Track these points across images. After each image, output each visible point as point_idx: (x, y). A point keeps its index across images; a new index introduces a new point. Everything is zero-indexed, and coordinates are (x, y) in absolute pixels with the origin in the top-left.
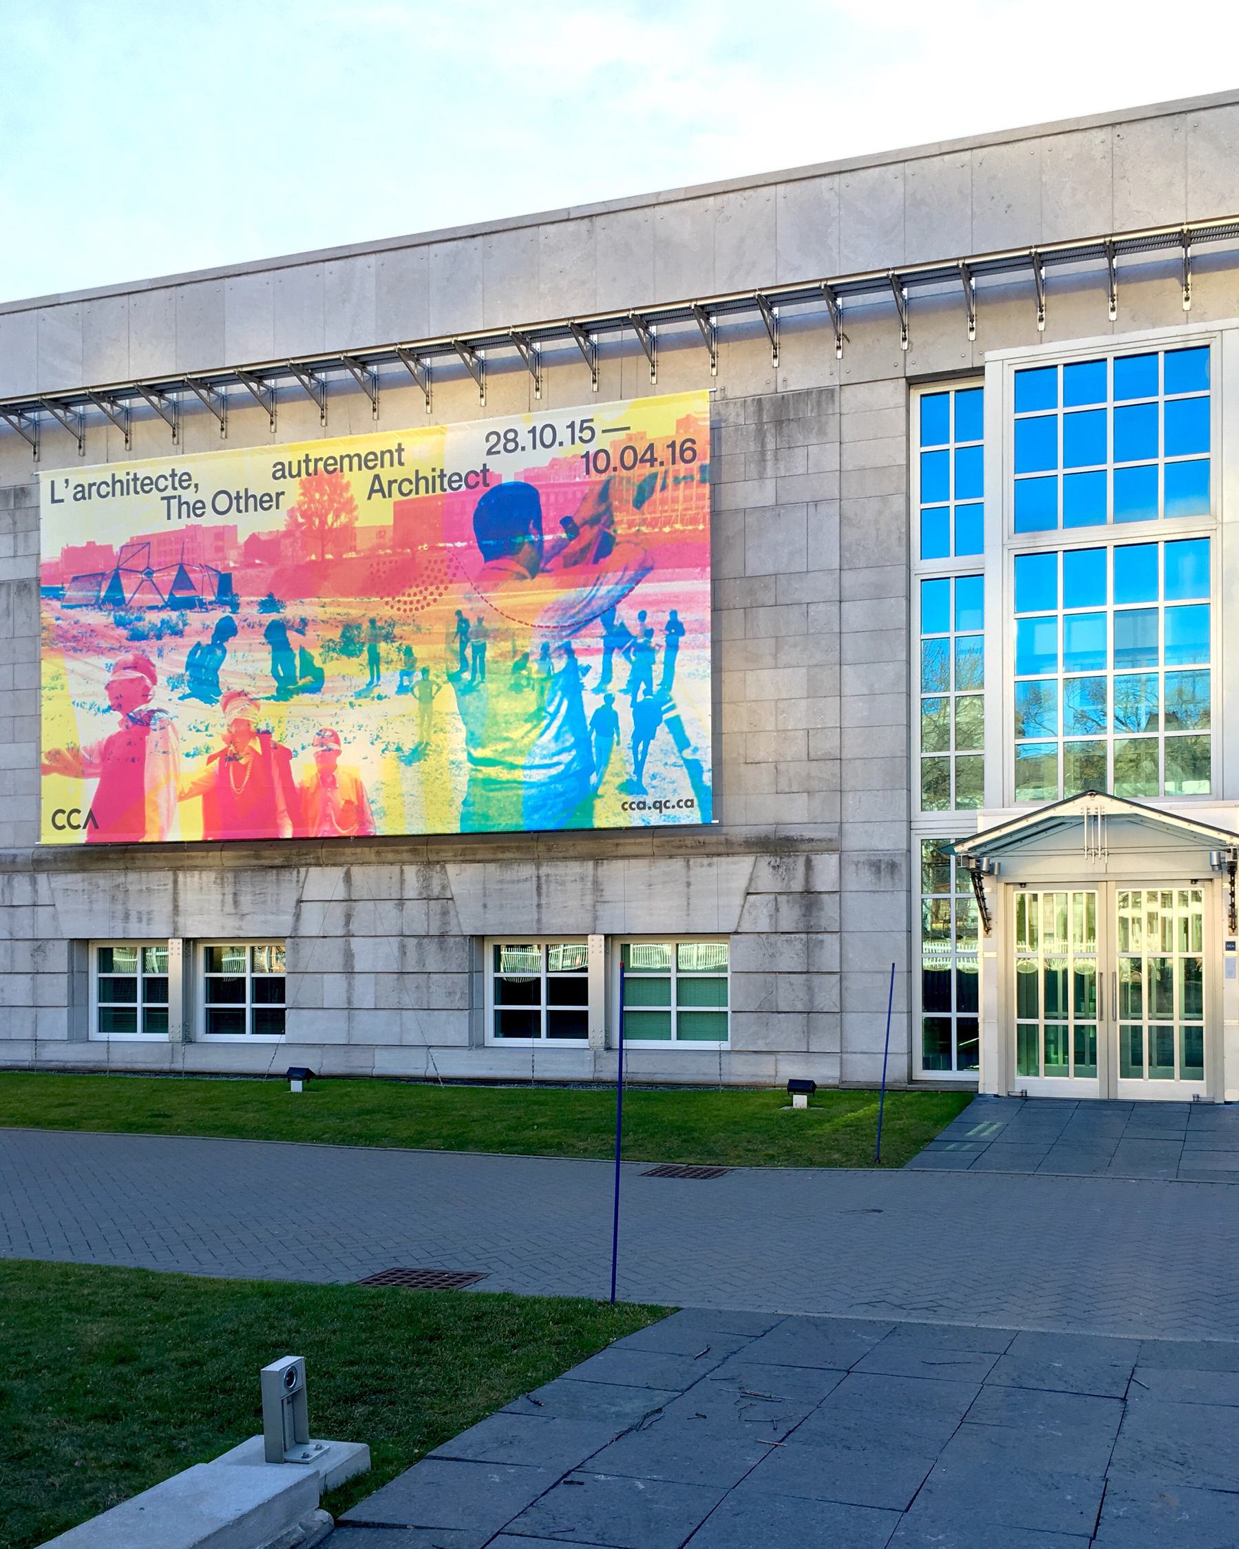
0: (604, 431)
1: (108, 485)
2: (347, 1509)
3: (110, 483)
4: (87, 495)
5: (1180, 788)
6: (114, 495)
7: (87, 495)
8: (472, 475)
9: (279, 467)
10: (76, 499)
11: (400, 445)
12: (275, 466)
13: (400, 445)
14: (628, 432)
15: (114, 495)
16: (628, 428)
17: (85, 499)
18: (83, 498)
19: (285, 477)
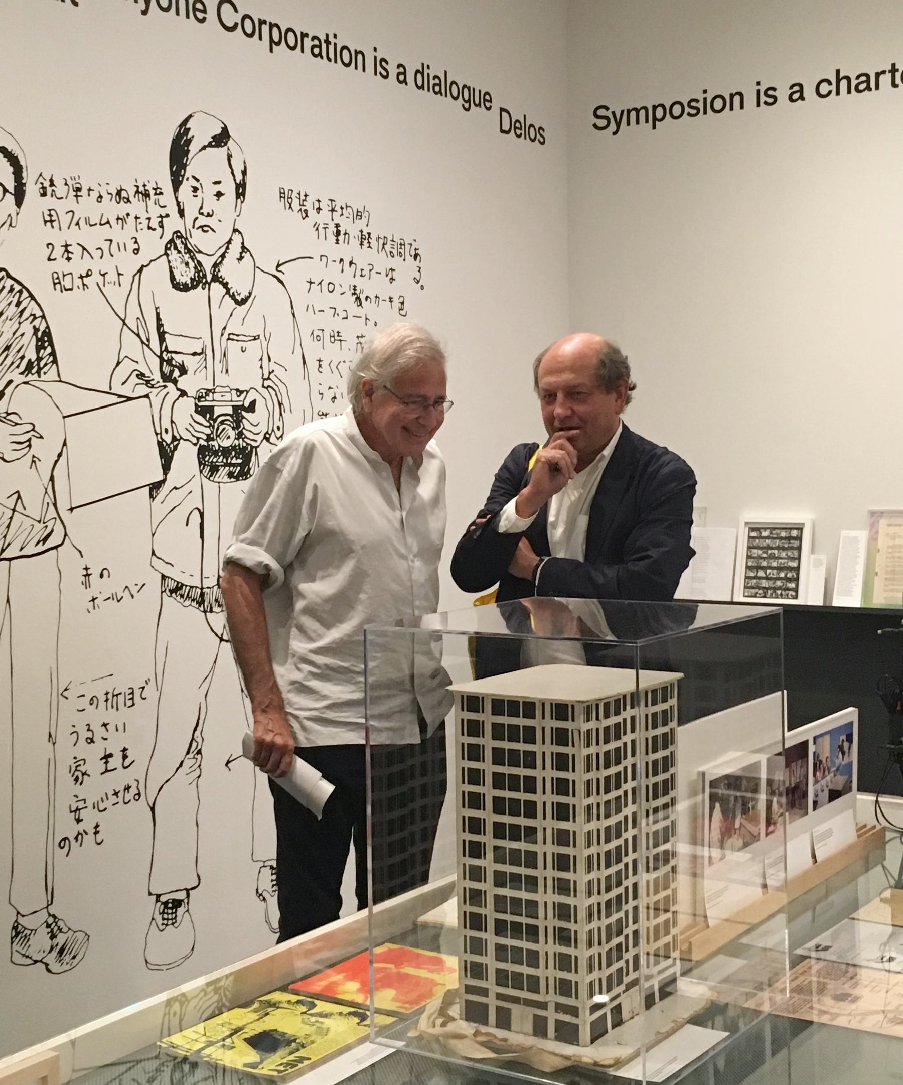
0: (360, 317)
1: (830, 83)
2: (425, 913)
3: (834, 81)
4: (873, 85)
5: (766, 956)
6: (838, 93)
7: (873, 85)
8: (196, 511)
9: (864, 78)
10: (791, 99)
11: (894, 65)
12: (791, 88)
13: (894, 65)
14: (645, 966)
15: (838, 93)
16: (191, 415)
17: (870, 90)
18: (869, 88)
19: (870, 90)
